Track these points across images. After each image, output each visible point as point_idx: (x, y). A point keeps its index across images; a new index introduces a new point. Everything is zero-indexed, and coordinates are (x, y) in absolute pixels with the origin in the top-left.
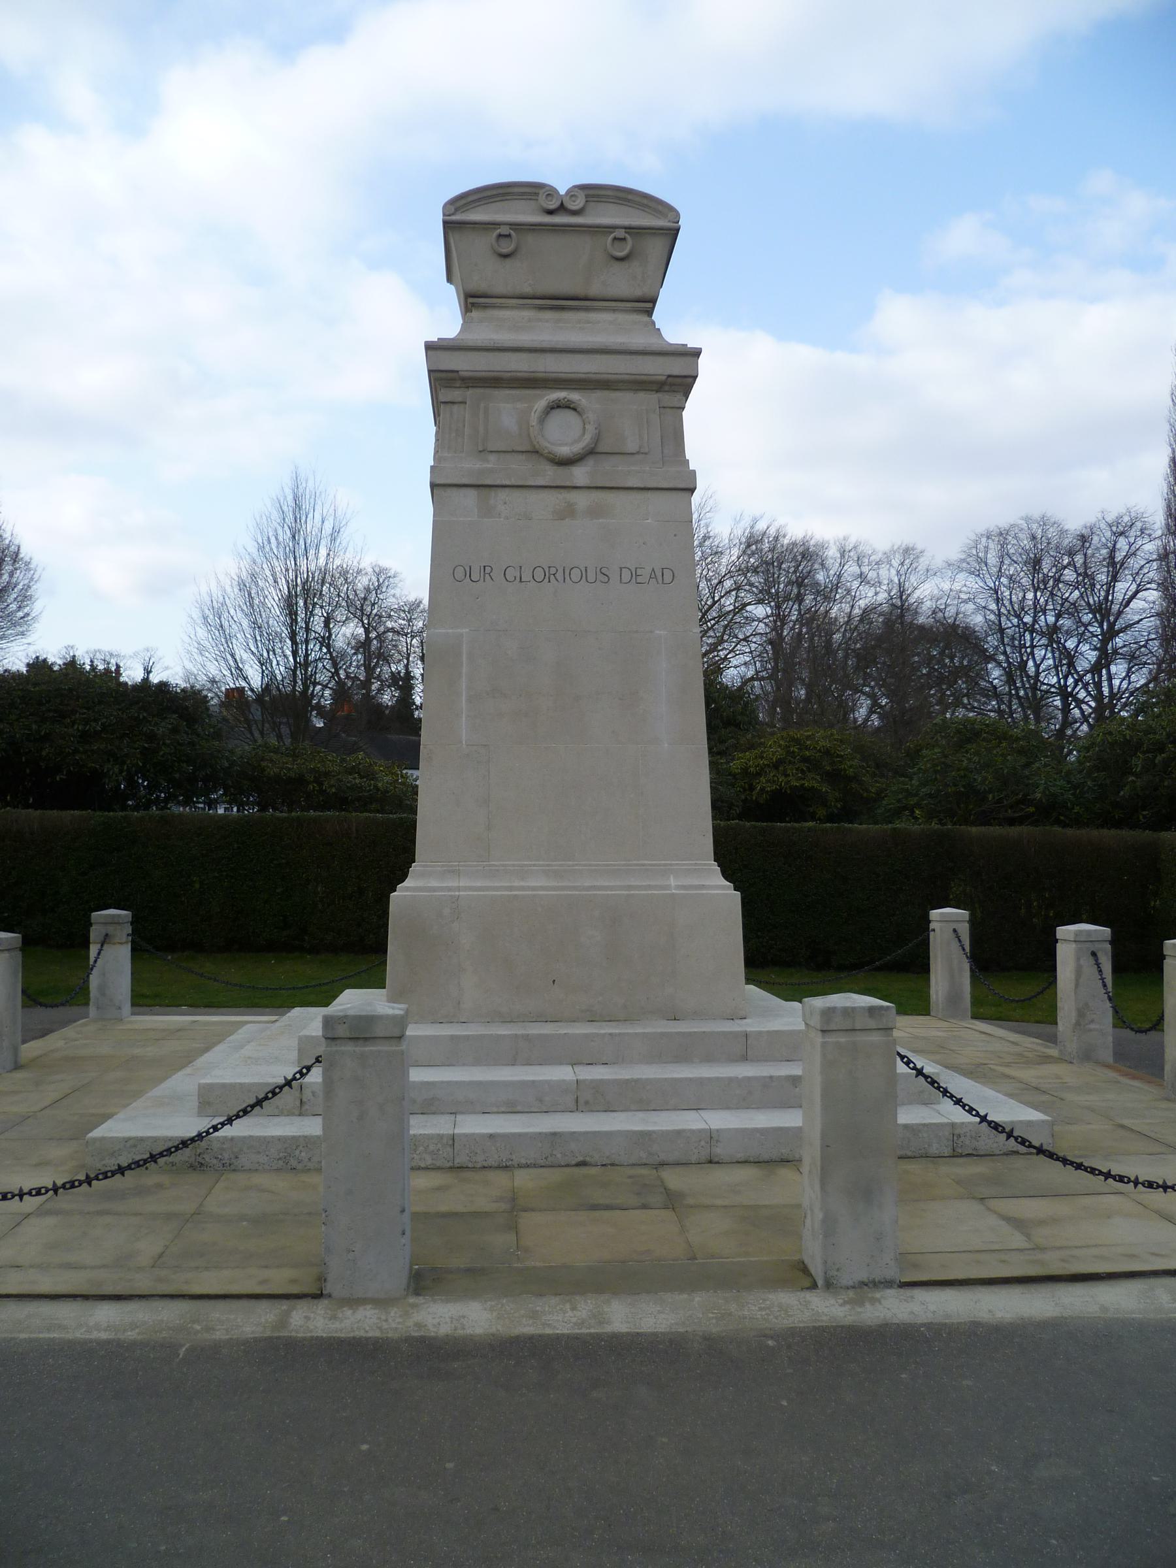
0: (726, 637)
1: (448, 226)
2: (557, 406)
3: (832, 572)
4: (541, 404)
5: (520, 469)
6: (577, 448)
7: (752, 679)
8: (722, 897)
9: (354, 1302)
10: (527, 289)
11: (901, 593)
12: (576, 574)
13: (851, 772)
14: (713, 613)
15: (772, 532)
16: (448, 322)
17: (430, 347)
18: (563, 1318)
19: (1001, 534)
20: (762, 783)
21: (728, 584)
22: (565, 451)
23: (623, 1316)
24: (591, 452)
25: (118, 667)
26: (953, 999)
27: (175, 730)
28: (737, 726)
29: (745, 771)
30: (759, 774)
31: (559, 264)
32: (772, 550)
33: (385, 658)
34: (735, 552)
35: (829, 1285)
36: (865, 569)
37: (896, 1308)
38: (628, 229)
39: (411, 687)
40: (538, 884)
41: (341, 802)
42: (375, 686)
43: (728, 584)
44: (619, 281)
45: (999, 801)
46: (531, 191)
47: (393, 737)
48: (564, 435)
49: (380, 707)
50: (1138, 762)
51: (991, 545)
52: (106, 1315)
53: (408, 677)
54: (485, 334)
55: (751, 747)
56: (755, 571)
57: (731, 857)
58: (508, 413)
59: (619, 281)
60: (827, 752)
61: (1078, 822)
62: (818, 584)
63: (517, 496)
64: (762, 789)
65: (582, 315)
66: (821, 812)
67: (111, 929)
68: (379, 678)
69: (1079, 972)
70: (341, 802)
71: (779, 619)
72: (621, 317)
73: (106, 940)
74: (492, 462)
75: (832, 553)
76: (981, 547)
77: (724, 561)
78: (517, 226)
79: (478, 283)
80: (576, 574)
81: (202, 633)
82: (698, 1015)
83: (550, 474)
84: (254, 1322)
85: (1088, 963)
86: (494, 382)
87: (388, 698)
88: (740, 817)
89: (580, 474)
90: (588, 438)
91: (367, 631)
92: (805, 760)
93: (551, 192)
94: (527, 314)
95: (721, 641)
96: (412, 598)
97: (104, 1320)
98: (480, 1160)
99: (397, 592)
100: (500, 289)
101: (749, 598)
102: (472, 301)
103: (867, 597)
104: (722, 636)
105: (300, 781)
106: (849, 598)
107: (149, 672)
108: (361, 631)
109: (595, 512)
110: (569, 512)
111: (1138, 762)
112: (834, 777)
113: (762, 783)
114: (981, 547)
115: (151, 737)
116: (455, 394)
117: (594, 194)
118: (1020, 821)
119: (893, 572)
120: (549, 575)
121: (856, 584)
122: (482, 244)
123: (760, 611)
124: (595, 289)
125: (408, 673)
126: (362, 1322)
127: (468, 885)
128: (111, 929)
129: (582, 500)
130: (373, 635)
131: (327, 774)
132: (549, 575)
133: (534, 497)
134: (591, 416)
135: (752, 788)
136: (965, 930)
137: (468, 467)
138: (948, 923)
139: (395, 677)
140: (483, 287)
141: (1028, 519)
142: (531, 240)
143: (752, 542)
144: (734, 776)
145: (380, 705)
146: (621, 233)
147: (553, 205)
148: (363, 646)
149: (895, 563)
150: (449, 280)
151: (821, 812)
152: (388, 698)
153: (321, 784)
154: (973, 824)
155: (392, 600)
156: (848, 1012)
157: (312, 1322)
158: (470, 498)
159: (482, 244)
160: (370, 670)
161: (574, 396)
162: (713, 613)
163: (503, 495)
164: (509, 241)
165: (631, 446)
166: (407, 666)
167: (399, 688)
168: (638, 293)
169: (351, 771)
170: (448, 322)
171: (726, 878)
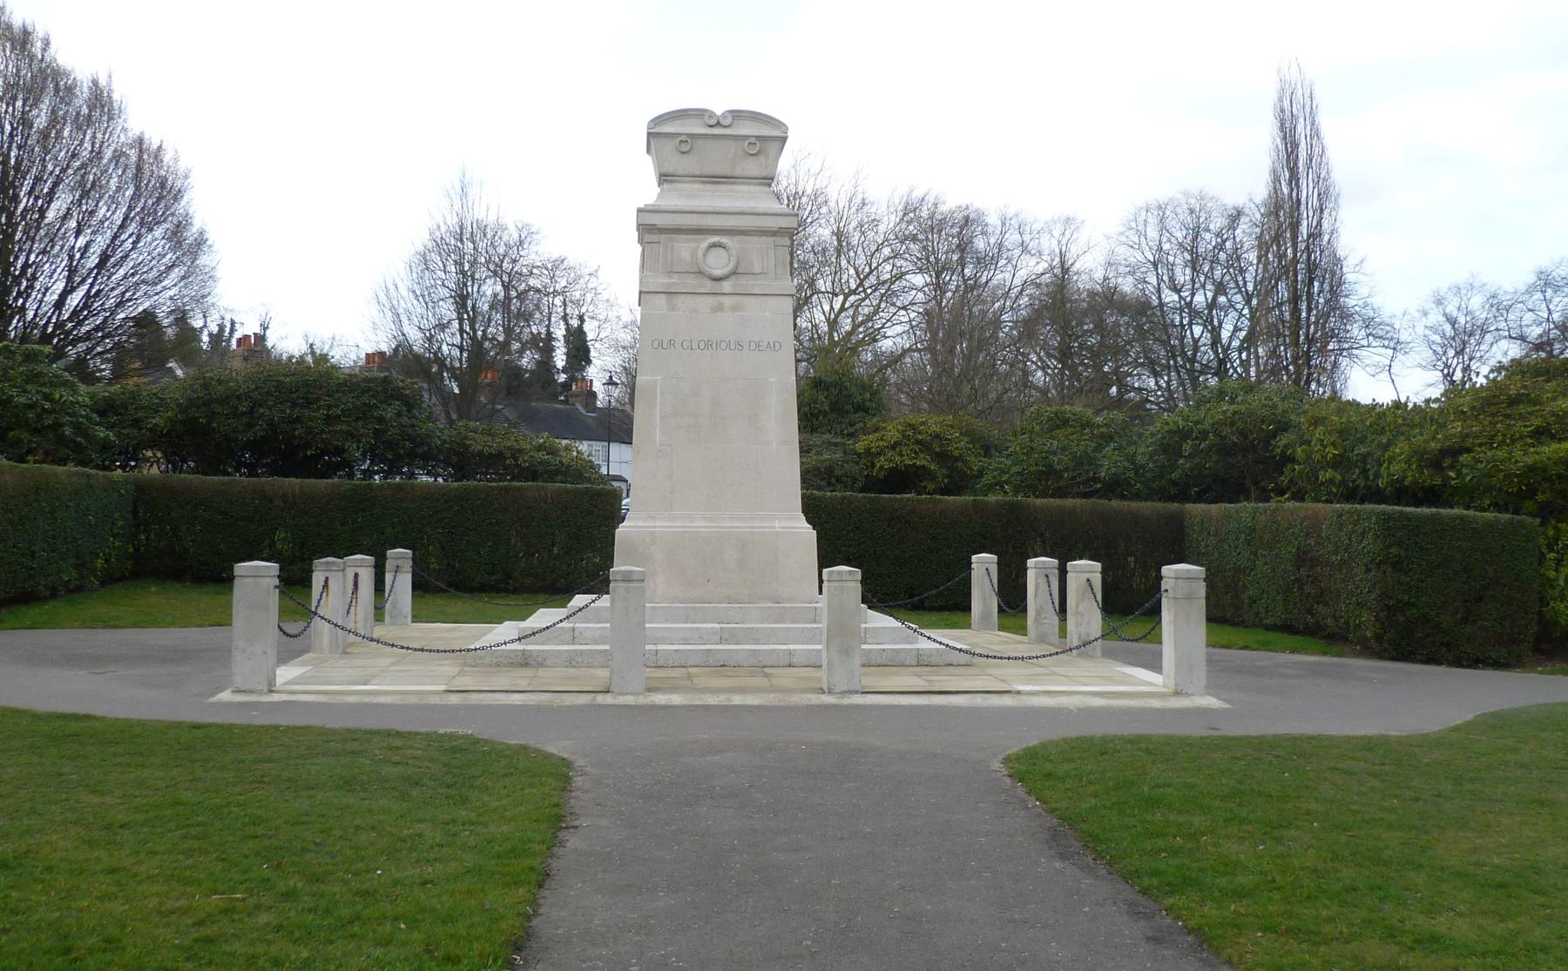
0: (883, 305)
1: (649, 135)
2: (714, 245)
3: (992, 241)
4: (705, 245)
5: (692, 282)
6: (725, 271)
7: (910, 350)
8: (808, 534)
9: (623, 694)
10: (697, 172)
11: (1062, 263)
12: (723, 345)
13: (956, 453)
14: (872, 280)
15: (931, 199)
16: (648, 191)
17: (639, 211)
18: (712, 700)
19: (1160, 207)
20: (881, 462)
21: (886, 251)
22: (718, 273)
23: (737, 700)
24: (734, 273)
25: (233, 323)
26: (985, 617)
27: (399, 415)
28: (866, 411)
29: (868, 451)
30: (879, 454)
31: (717, 158)
32: (931, 217)
33: (527, 317)
34: (894, 219)
35: (830, 692)
36: (1027, 238)
37: (858, 699)
38: (757, 137)
39: (552, 349)
40: (699, 524)
41: (532, 474)
42: (516, 346)
43: (886, 251)
44: (752, 168)
45: (1073, 478)
46: (700, 114)
48: (718, 263)
49: (517, 372)
50: (1187, 448)
51: (1150, 220)
52: (517, 699)
55: (877, 430)
56: (914, 239)
57: (812, 510)
58: (684, 249)
59: (752, 168)
60: (937, 436)
61: (1138, 496)
62: (977, 252)
63: (690, 300)
64: (881, 467)
65: (729, 187)
66: (931, 487)
67: (400, 562)
68: (519, 340)
69: (1037, 587)
70: (532, 474)
71: (940, 287)
72: (752, 188)
73: (397, 570)
74: (675, 279)
75: (993, 220)
76: (1140, 220)
77: (882, 228)
78: (691, 136)
79: (668, 169)
80: (723, 345)
81: (374, 311)
82: (789, 600)
83: (709, 286)
84: (583, 699)
85: (1044, 586)
86: (678, 231)
87: (527, 361)
88: (863, 490)
89: (727, 286)
90: (731, 265)
91: (506, 287)
92: (918, 442)
93: (712, 114)
94: (696, 186)
95: (876, 312)
96: (555, 256)
97: (517, 699)
98: (670, 663)
99: (540, 249)
100: (681, 172)
101: (909, 266)
102: (664, 178)
104: (879, 306)
105: (499, 457)
106: (1010, 267)
107: (265, 329)
108: (499, 288)
109: (734, 308)
110: (720, 308)
111: (1187, 448)
112: (943, 457)
113: (881, 462)
114: (1140, 220)
115: (381, 420)
116: (654, 237)
117: (737, 115)
119: (1055, 243)
120: (708, 345)
121: (1017, 252)
122: (669, 146)
123: (918, 280)
124: (738, 172)
125: (549, 334)
126: (629, 700)
127: (660, 525)
128: (400, 562)
129: (727, 301)
130: (514, 294)
131: (520, 451)
132: (708, 345)
133: (700, 299)
134: (734, 252)
135: (873, 465)
136: (1097, 579)
137: (660, 281)
138: (984, 565)
139: (535, 339)
140: (671, 171)
141: (1186, 194)
142: (699, 142)
143: (909, 211)
144: (859, 455)
145: (519, 368)
146: (753, 140)
147: (713, 122)
149: (1056, 234)
150: (648, 151)
151: (931, 487)
152: (527, 361)
153: (516, 459)
154: (1199, 499)
155: (533, 256)
156: (839, 573)
157: (608, 699)
158: (662, 300)
159: (669, 146)
160: (508, 331)
161: (724, 240)
162: (872, 280)
163: (681, 298)
164: (687, 144)
165: (757, 269)
166: (548, 326)
168: (763, 174)
169: (540, 448)
170: (648, 191)
171: (808, 521)
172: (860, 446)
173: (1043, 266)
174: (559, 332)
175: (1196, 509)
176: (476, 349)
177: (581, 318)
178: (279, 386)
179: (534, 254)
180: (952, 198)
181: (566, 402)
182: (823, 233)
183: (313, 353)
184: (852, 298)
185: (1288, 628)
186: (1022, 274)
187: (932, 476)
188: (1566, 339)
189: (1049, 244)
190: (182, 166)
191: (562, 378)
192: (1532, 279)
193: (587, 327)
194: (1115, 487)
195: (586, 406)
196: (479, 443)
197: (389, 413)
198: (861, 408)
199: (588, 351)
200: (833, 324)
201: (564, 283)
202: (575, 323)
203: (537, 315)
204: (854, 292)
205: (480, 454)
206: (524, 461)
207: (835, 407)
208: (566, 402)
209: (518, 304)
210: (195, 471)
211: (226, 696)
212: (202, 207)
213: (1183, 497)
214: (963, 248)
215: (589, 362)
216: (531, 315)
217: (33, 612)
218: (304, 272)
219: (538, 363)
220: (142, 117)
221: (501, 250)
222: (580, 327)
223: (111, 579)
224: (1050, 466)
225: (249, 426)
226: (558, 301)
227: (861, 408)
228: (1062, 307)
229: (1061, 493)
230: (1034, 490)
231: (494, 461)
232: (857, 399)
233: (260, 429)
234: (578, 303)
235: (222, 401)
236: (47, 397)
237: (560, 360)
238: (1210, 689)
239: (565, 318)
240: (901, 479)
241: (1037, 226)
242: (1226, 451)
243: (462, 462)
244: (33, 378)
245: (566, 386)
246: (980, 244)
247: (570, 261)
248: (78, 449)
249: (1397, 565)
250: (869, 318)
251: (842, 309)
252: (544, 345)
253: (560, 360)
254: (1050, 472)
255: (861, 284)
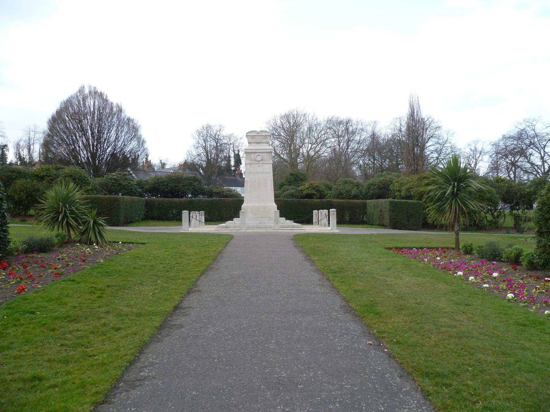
5: (254, 162)
8: (275, 206)
20: (304, 192)
21: (323, 132)
31: (258, 139)
33: (222, 151)
41: (226, 196)
42: (219, 160)
43: (323, 132)
46: (255, 131)
47: (227, 177)
48: (259, 158)
49: (220, 167)
53: (229, 157)
54: (250, 148)
57: (276, 201)
58: (253, 156)
60: (317, 186)
66: (315, 197)
70: (226, 196)
75: (354, 121)
77: (322, 125)
83: (257, 162)
87: (223, 163)
89: (260, 162)
91: (217, 144)
102: (249, 143)
103: (364, 135)
105: (219, 193)
109: (262, 166)
111: (372, 188)
112: (318, 191)
113: (304, 192)
115: (194, 186)
117: (262, 131)
118: (350, 199)
123: (333, 140)
125: (229, 156)
127: (249, 205)
129: (260, 165)
137: (249, 162)
138: (185, 213)
139: (225, 157)
148: (216, 148)
151: (315, 197)
164: (253, 137)
167: (227, 161)
172: (300, 189)
173: (368, 135)
174: (232, 155)
175: (368, 201)
176: (208, 161)
177: (238, 151)
178: (173, 179)
179: (224, 133)
180: (343, 116)
181: (234, 176)
182: (305, 128)
183: (161, 163)
184: (314, 145)
185: (379, 225)
186: (363, 137)
187: (316, 195)
188: (1, 226)
189: (370, 129)
190: (139, 124)
191: (233, 168)
192: (501, 137)
193: (240, 153)
194: (355, 197)
195: (240, 177)
196: (215, 190)
197: (196, 184)
198: (301, 180)
199: (241, 160)
200: (308, 152)
201: (233, 141)
202: (237, 152)
203: (226, 151)
204: (314, 144)
205: (215, 192)
206: (224, 194)
207: (295, 180)
208: (234, 176)
209: (219, 148)
210: (160, 197)
211: (182, 231)
212: (144, 133)
213: (366, 198)
214: (347, 129)
215: (241, 164)
216: (224, 150)
217: (135, 224)
218: (167, 147)
219: (226, 165)
220: (128, 112)
221: (215, 132)
222: (238, 153)
223: (142, 220)
224: (341, 192)
225: (167, 188)
226: (232, 146)
227: (301, 180)
228: (375, 146)
229: (343, 198)
230: (337, 198)
231: (218, 194)
232: (301, 178)
233: (169, 188)
234: (238, 147)
235: (161, 182)
236: (129, 183)
237: (232, 163)
238: (337, 229)
239: (234, 151)
240: (309, 196)
241: (367, 123)
242: (380, 188)
243: (210, 194)
244: (126, 179)
245: (234, 171)
246: (351, 129)
247: (235, 134)
248: (135, 193)
249: (393, 211)
250: (319, 151)
251: (311, 149)
252: (228, 159)
253: (232, 163)
254: (341, 194)
255: (316, 141)
